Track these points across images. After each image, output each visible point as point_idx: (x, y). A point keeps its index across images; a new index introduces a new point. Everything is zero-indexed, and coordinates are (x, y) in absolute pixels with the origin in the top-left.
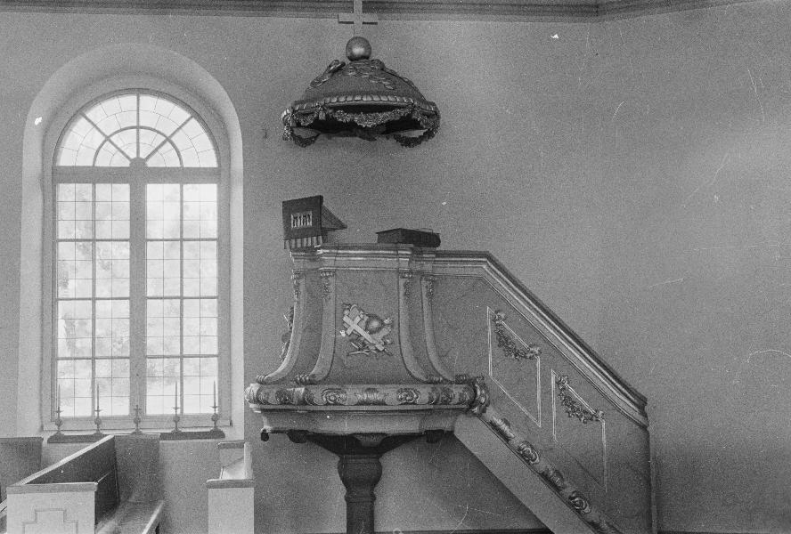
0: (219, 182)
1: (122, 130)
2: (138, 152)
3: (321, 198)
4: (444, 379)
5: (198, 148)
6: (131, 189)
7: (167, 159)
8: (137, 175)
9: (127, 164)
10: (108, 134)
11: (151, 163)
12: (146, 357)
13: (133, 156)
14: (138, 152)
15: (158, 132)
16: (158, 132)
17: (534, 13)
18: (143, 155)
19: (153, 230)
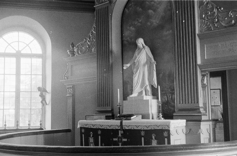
0: (42, 58)
1: (30, 49)
2: (22, 50)
3: (149, 100)
4: (142, 87)
5: (36, 48)
6: (16, 59)
7: (26, 51)
8: (18, 56)
9: (15, 52)
10: (9, 43)
11: (22, 52)
12: (174, 116)
13: (17, 50)
14: (22, 50)
15: (25, 43)
16: (25, 43)
17: (10, 153)
18: (20, 50)
19: (22, 72)
